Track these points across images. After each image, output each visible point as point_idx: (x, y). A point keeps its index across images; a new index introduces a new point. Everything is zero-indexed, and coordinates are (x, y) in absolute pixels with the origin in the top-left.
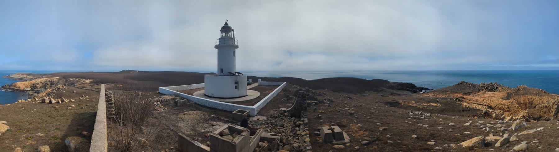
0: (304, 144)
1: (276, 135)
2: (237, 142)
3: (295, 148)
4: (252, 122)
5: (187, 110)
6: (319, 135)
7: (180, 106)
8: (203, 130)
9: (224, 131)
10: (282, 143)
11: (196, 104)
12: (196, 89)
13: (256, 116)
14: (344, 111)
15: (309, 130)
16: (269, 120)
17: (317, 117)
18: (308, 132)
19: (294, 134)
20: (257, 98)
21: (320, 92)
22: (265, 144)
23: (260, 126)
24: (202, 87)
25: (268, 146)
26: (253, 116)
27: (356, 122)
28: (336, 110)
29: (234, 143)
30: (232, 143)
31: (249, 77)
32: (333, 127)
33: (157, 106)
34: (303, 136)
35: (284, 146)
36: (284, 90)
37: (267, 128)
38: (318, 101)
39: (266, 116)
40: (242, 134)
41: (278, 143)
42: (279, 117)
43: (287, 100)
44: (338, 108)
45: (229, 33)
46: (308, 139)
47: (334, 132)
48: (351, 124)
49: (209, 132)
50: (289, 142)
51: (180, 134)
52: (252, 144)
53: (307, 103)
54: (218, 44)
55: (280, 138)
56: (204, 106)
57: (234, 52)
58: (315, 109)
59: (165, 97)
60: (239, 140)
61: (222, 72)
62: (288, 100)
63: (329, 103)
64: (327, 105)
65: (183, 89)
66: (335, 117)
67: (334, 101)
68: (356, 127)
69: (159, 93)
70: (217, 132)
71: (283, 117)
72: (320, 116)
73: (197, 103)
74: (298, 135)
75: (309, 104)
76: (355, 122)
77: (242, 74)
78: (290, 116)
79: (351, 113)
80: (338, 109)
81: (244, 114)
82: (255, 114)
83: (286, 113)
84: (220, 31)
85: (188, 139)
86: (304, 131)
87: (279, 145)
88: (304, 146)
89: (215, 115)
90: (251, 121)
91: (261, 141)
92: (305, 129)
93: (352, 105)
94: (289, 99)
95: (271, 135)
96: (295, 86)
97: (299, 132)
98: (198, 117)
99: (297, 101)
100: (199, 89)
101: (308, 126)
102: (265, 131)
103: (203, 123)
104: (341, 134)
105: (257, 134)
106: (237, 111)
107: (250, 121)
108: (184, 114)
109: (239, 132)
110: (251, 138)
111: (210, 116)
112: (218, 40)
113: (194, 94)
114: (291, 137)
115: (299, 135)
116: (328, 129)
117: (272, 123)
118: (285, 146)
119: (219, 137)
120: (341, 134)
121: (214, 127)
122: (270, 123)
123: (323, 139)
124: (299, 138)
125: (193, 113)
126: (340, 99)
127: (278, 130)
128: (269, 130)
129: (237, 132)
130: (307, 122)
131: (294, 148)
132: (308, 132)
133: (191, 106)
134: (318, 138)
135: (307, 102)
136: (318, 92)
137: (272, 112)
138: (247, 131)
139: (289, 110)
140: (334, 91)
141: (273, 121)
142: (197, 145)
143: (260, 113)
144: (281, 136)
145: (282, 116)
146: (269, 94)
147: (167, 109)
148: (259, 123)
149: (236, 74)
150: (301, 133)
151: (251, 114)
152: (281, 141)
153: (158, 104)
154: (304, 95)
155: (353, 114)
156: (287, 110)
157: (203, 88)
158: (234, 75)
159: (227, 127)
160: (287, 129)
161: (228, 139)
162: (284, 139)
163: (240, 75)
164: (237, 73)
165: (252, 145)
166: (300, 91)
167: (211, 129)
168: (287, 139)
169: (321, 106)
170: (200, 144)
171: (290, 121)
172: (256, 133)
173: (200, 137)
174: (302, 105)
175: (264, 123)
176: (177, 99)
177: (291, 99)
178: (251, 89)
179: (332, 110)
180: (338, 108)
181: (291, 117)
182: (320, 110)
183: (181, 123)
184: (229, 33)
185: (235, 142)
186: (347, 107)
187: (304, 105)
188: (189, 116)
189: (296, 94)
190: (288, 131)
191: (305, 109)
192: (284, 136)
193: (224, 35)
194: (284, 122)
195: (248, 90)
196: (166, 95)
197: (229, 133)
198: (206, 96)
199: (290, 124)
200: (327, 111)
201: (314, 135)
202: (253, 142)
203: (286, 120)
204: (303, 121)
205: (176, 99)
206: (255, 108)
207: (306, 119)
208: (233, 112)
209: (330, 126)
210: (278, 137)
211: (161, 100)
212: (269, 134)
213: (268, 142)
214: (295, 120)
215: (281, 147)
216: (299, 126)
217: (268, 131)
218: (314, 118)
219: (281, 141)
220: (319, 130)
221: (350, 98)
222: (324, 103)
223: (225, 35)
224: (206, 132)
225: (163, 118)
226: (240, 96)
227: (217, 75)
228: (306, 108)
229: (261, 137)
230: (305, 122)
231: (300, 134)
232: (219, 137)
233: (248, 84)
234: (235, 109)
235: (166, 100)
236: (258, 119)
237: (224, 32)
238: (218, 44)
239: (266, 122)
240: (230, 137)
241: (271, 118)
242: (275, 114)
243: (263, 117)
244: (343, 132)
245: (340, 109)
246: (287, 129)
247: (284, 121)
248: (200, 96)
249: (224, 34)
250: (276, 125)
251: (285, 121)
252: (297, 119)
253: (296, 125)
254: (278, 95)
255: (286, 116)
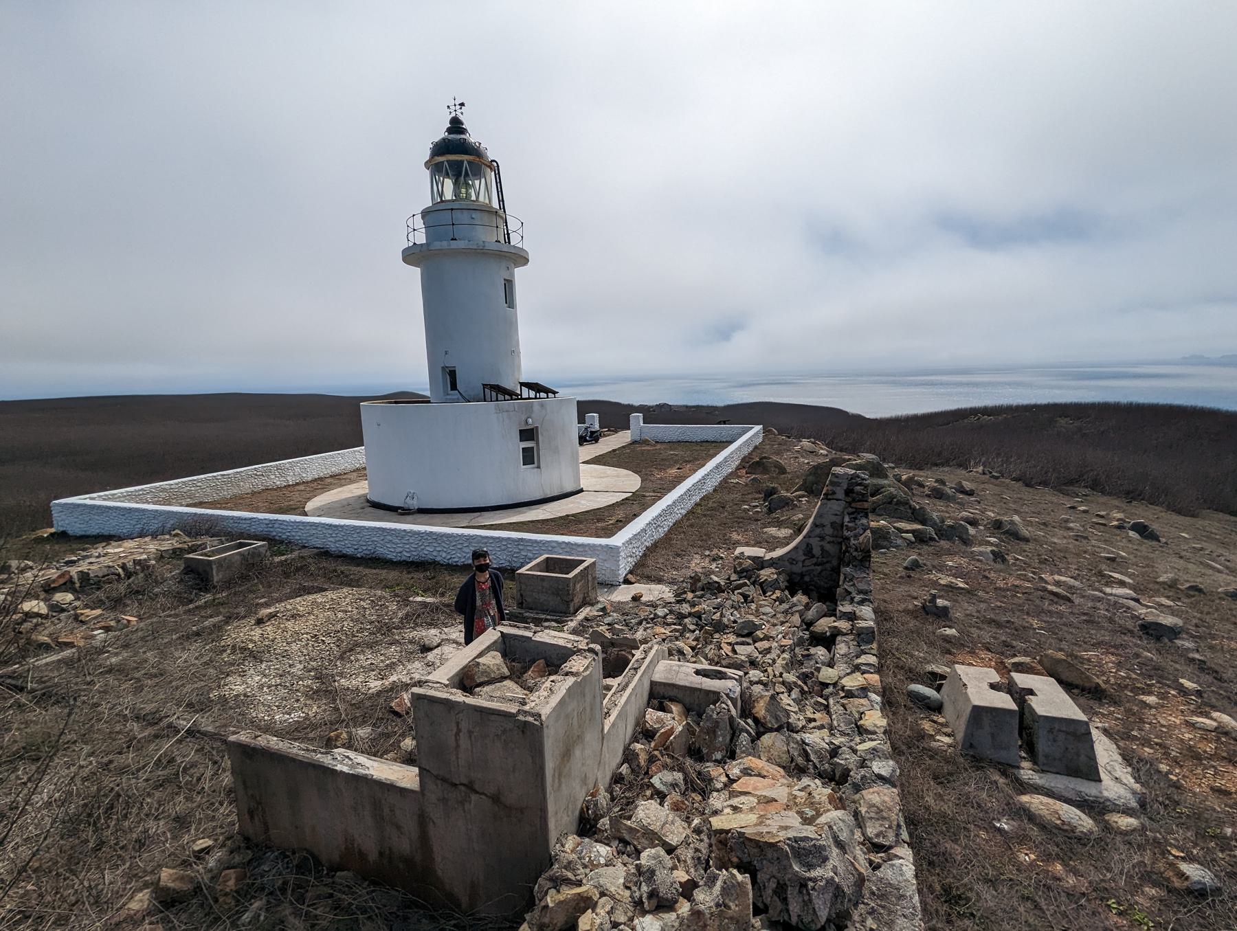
0: (857, 739)
1: (721, 676)
2: (545, 711)
3: (812, 757)
4: (609, 608)
5: (276, 595)
6: (938, 708)
7: (228, 584)
8: (375, 685)
9: (480, 660)
10: (749, 721)
11: (325, 554)
12: (321, 479)
13: (627, 582)
14: (1099, 600)
15: (879, 670)
16: (684, 600)
17: (924, 607)
18: (876, 677)
19: (805, 677)
20: (626, 499)
21: (942, 482)
22: (672, 721)
23: (645, 630)
24: (349, 467)
25: (689, 730)
26: (611, 586)
27: (1199, 693)
28: (1045, 590)
29: (533, 715)
30: (521, 717)
31: (584, 408)
32: (1023, 680)
33: (48, 623)
34: (850, 694)
35: (759, 735)
36: (753, 463)
37: (677, 639)
38: (934, 525)
39: (672, 582)
40: (566, 667)
41: (731, 717)
42: (731, 587)
43: (765, 509)
44: (1057, 577)
45: (477, 182)
46: (875, 719)
47: (1032, 710)
48: (1150, 693)
49: (406, 687)
50: (784, 720)
51: (243, 737)
52: (612, 718)
53: (874, 531)
54: (421, 238)
55: (742, 694)
56: (375, 561)
57: (509, 285)
58: (915, 566)
59: (114, 549)
60: (555, 700)
61: (454, 386)
62: (771, 511)
63: (992, 540)
64: (981, 554)
65: (236, 491)
66: (1035, 623)
67: (1025, 532)
68: (1192, 726)
69: (62, 536)
70: (443, 674)
71: (752, 591)
72: (940, 602)
73: (333, 547)
74: (826, 685)
75: (881, 538)
76: (1183, 691)
77: (554, 393)
78: (783, 585)
79: (1158, 625)
80: (1058, 584)
81: (571, 575)
82: (622, 573)
83: (762, 572)
84: (427, 164)
85: (295, 749)
86: (857, 668)
87: (735, 732)
88: (855, 751)
89: (434, 595)
90: (603, 609)
91: (656, 702)
92: (859, 661)
93: (1161, 579)
94: (775, 505)
95: (698, 672)
96: (805, 443)
97: (827, 674)
98: (342, 620)
99: (819, 515)
100: (339, 479)
101: (875, 646)
102: (670, 654)
103: (370, 646)
104: (1077, 734)
105: (636, 669)
106: (538, 564)
107: (600, 606)
108: (260, 622)
109: (554, 661)
110: (608, 688)
111: (406, 602)
112: (419, 219)
113: (310, 506)
114: (790, 691)
115: (831, 689)
116: (993, 686)
117: (698, 616)
118: (767, 739)
119: (458, 696)
120: (1077, 734)
121: (431, 656)
122: (690, 614)
123: (960, 736)
124: (831, 701)
125: (314, 602)
126: (1069, 529)
127: (727, 649)
128: (687, 650)
129: (542, 662)
130: (872, 623)
131: (806, 755)
132: (874, 678)
133: (298, 570)
134: (927, 726)
135: (873, 524)
136: (929, 479)
137: (697, 564)
138: (591, 650)
139: (780, 558)
140: (1027, 481)
141: (704, 606)
142: (345, 769)
143: (642, 571)
144: (745, 685)
145: (745, 584)
146: (680, 483)
147: (140, 619)
148: (643, 615)
149: (525, 392)
150: (840, 678)
151: (601, 574)
152: (746, 706)
153: (58, 609)
154: (858, 488)
155: (1174, 632)
156: (767, 558)
157: (360, 473)
158: (511, 395)
159: (495, 642)
160: (768, 650)
161: (503, 699)
162: (756, 701)
163: (543, 395)
164: (530, 386)
165: (613, 725)
166: (838, 470)
167: (416, 669)
168: (773, 697)
169: (950, 553)
170: (362, 759)
171: (786, 612)
172: (627, 662)
173: (364, 723)
174: (848, 539)
175: (665, 617)
176: (204, 546)
177: (786, 503)
178: (598, 460)
179: (1017, 582)
180: (1057, 577)
181: (787, 592)
182: (940, 571)
183: (243, 674)
184: (477, 182)
185: (537, 709)
186: (1122, 584)
187: (856, 537)
188: (290, 624)
189: (815, 482)
190: (774, 661)
191: (864, 560)
192: (760, 682)
193: (449, 194)
194: (757, 613)
195: (583, 467)
196: (119, 538)
197: (506, 671)
198: (377, 507)
199: (782, 623)
200: (984, 582)
201: (910, 704)
202: (618, 708)
203: (761, 606)
204: (852, 617)
205: (192, 550)
206: (618, 548)
207: (866, 611)
208: (520, 568)
209: (1001, 668)
210: (730, 684)
211: (84, 576)
212: (690, 668)
213: (687, 710)
214: (807, 607)
215: (744, 738)
216: (828, 641)
217: (684, 654)
218: (907, 611)
219: (746, 706)
220: (935, 680)
221: (1142, 529)
222: (966, 541)
223: (456, 193)
224: (392, 689)
225: (111, 679)
226: (549, 494)
227: (429, 402)
228: (866, 557)
229: (653, 684)
230: (862, 624)
231: (835, 685)
232: (458, 696)
233: (582, 440)
234: (530, 555)
235: (124, 567)
236: (636, 598)
237: (447, 175)
238: (421, 238)
239: (671, 612)
240: (511, 688)
241: (693, 592)
242: (713, 573)
243: (659, 587)
244: (1095, 733)
245: (1071, 587)
246: (768, 650)
247: (753, 606)
248: (345, 509)
249: (449, 185)
250: (719, 627)
251: (762, 610)
252: (817, 607)
253: (811, 633)
254: (724, 485)
255: (764, 587)
